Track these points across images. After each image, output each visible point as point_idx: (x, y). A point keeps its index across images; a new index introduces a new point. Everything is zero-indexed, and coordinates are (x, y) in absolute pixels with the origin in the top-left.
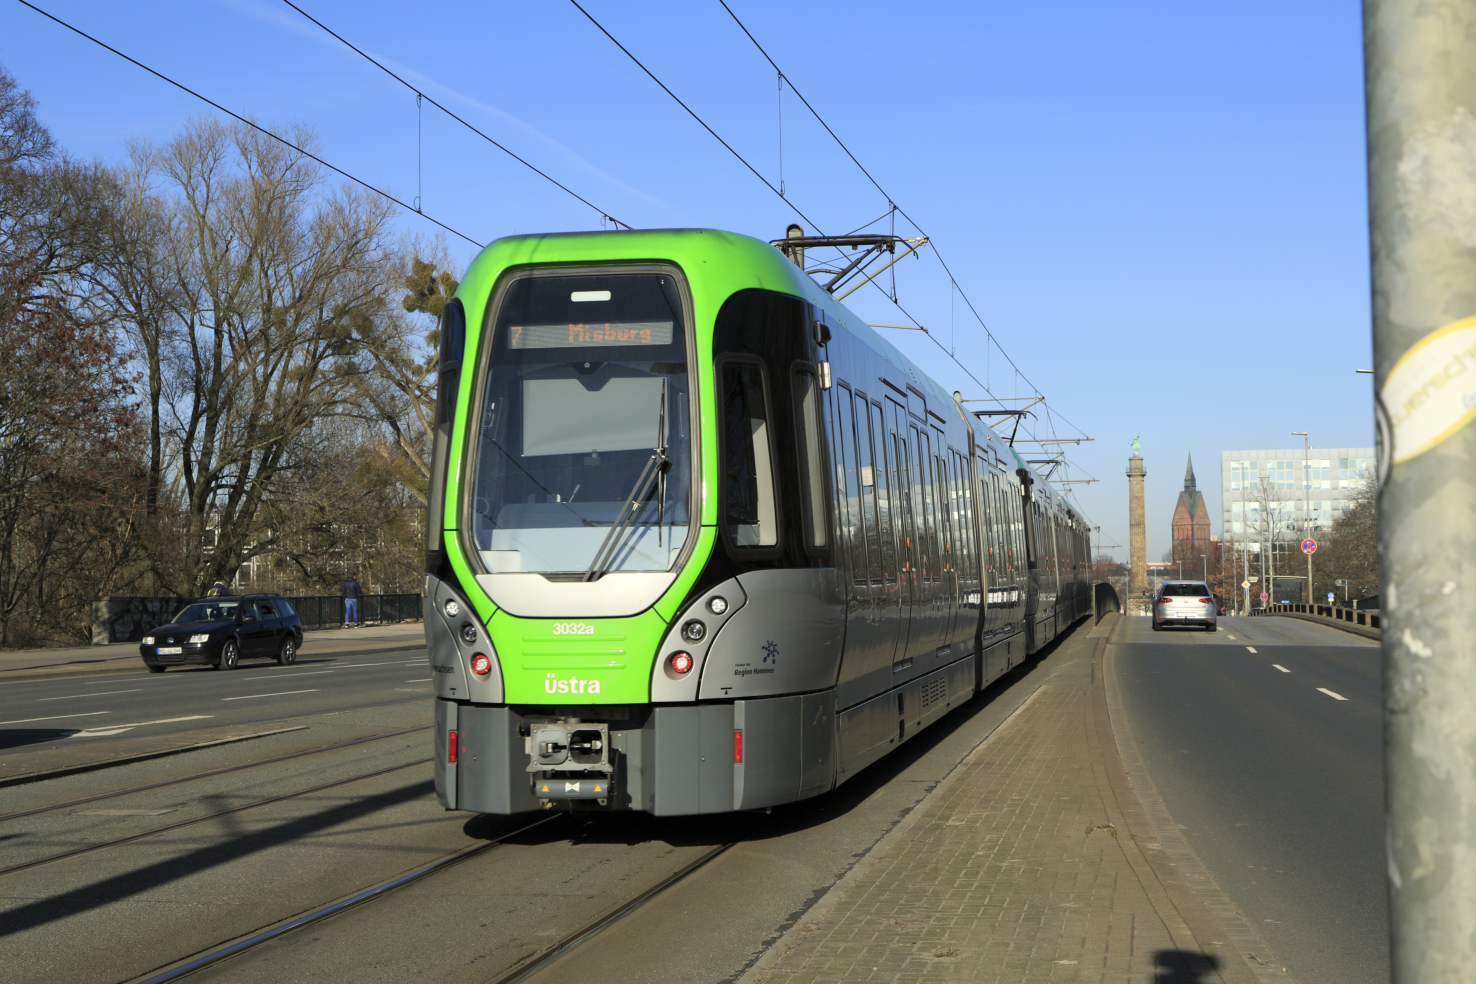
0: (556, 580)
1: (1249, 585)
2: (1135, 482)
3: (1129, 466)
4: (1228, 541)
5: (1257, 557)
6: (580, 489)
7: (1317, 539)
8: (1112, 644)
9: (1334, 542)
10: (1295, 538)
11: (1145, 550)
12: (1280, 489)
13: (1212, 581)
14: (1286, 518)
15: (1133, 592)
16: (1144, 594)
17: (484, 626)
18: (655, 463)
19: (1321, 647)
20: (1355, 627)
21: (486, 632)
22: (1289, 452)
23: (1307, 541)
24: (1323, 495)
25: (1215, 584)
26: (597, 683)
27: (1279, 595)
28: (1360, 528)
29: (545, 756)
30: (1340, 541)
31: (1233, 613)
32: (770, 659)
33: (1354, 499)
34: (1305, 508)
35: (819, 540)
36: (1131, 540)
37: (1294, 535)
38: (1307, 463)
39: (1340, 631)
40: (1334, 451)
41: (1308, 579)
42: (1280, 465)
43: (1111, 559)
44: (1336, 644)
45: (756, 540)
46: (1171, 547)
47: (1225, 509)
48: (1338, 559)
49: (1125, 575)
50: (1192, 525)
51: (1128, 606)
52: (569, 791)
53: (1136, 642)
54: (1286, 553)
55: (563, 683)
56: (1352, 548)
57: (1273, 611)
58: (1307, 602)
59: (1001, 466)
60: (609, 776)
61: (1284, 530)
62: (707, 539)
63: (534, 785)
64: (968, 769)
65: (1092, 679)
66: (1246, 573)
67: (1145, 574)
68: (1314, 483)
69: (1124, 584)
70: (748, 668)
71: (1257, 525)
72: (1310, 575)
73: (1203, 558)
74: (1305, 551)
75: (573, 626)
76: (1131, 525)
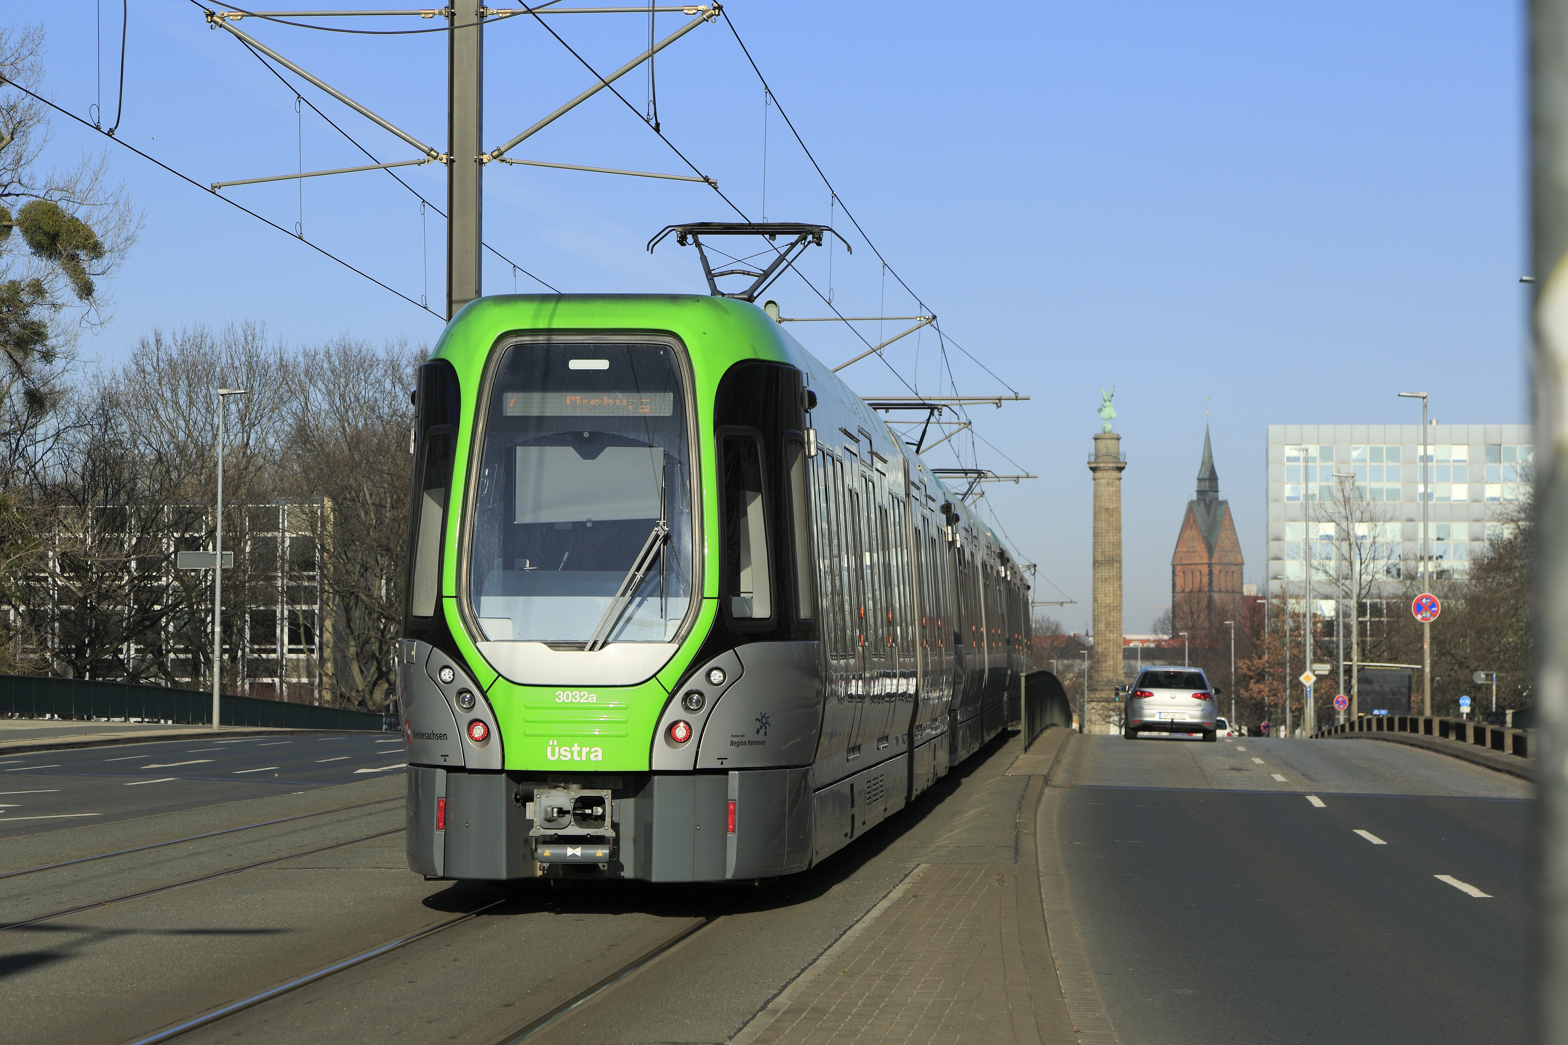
0: (557, 648)
1: (1314, 679)
2: (1104, 482)
3: (1093, 450)
4: (1277, 596)
5: (1329, 627)
6: (568, 557)
7: (1442, 594)
8: (1055, 786)
9: (1474, 601)
10: (1400, 593)
11: (1120, 611)
12: (1374, 499)
13: (1245, 670)
14: (1385, 554)
15: (1096, 690)
16: (1117, 694)
17: (484, 694)
18: (657, 536)
19: (1445, 797)
20: (1508, 761)
21: (486, 699)
22: (1393, 430)
23: (1422, 598)
24: (1455, 512)
25: (1251, 677)
26: (600, 750)
27: (1369, 699)
28: (1521, 575)
29: (549, 820)
30: (1485, 600)
31: (1283, 732)
32: (762, 731)
33: (1512, 520)
34: (1421, 535)
35: (804, 612)
36: (1095, 590)
37: (1400, 586)
38: (1425, 451)
39: (1480, 769)
40: (1477, 430)
41: (1422, 670)
42: (1376, 455)
43: (1057, 627)
44: (1471, 792)
45: (749, 613)
46: (1169, 604)
47: (1271, 536)
48: (1480, 632)
49: (1082, 657)
50: (1210, 565)
51: (1087, 716)
52: (570, 856)
53: (1100, 784)
54: (1384, 619)
55: (565, 750)
56: (1506, 613)
57: (1357, 728)
58: (1421, 712)
59: (879, 465)
60: (611, 841)
61: (1381, 577)
62: (709, 610)
63: (536, 850)
64: (777, 1021)
65: (1017, 852)
66: (1309, 655)
67: (1121, 656)
68: (1438, 489)
69: (1081, 675)
70: (743, 739)
71: (1332, 565)
72: (1428, 662)
73: (1229, 628)
74: (1419, 617)
75: (576, 694)
76: (1095, 563)
